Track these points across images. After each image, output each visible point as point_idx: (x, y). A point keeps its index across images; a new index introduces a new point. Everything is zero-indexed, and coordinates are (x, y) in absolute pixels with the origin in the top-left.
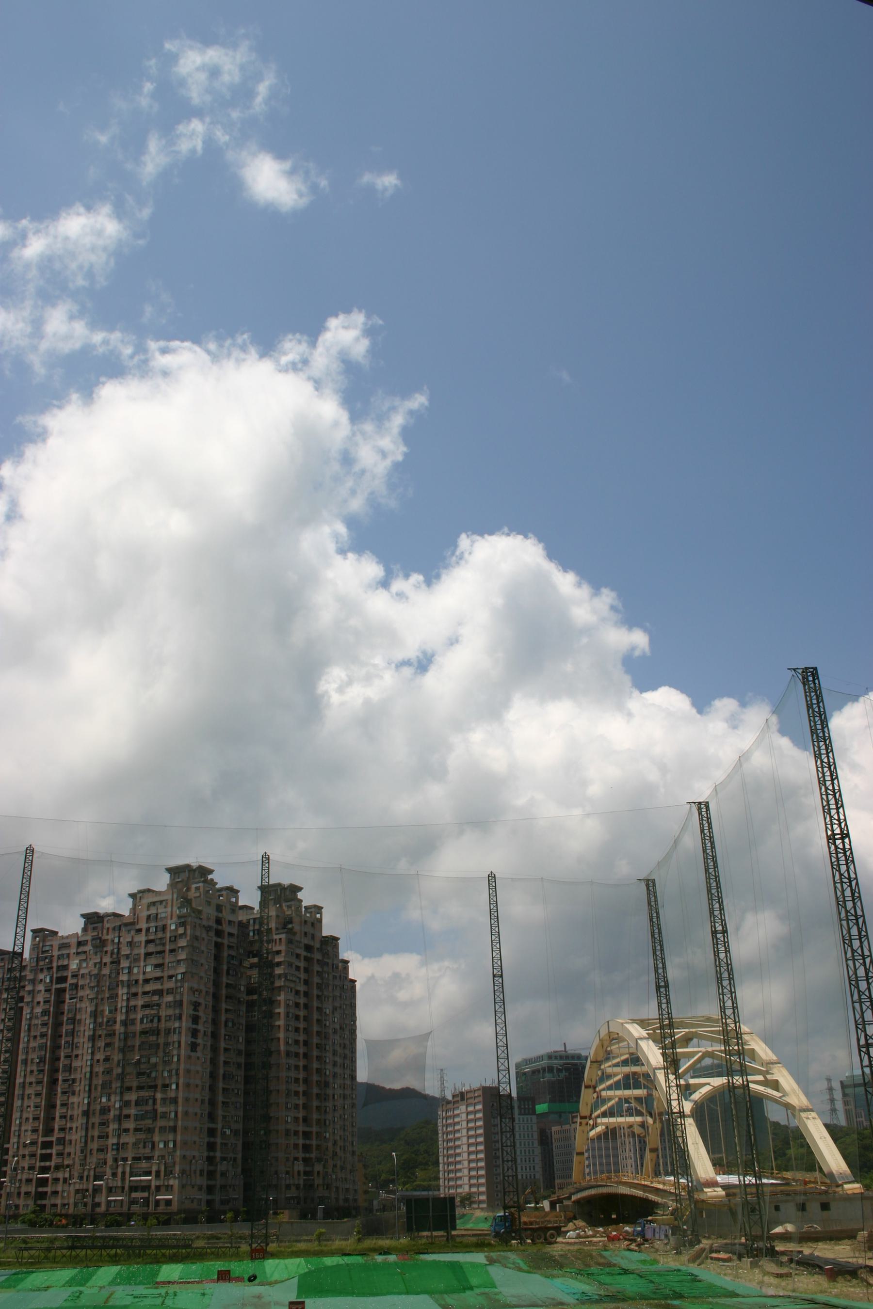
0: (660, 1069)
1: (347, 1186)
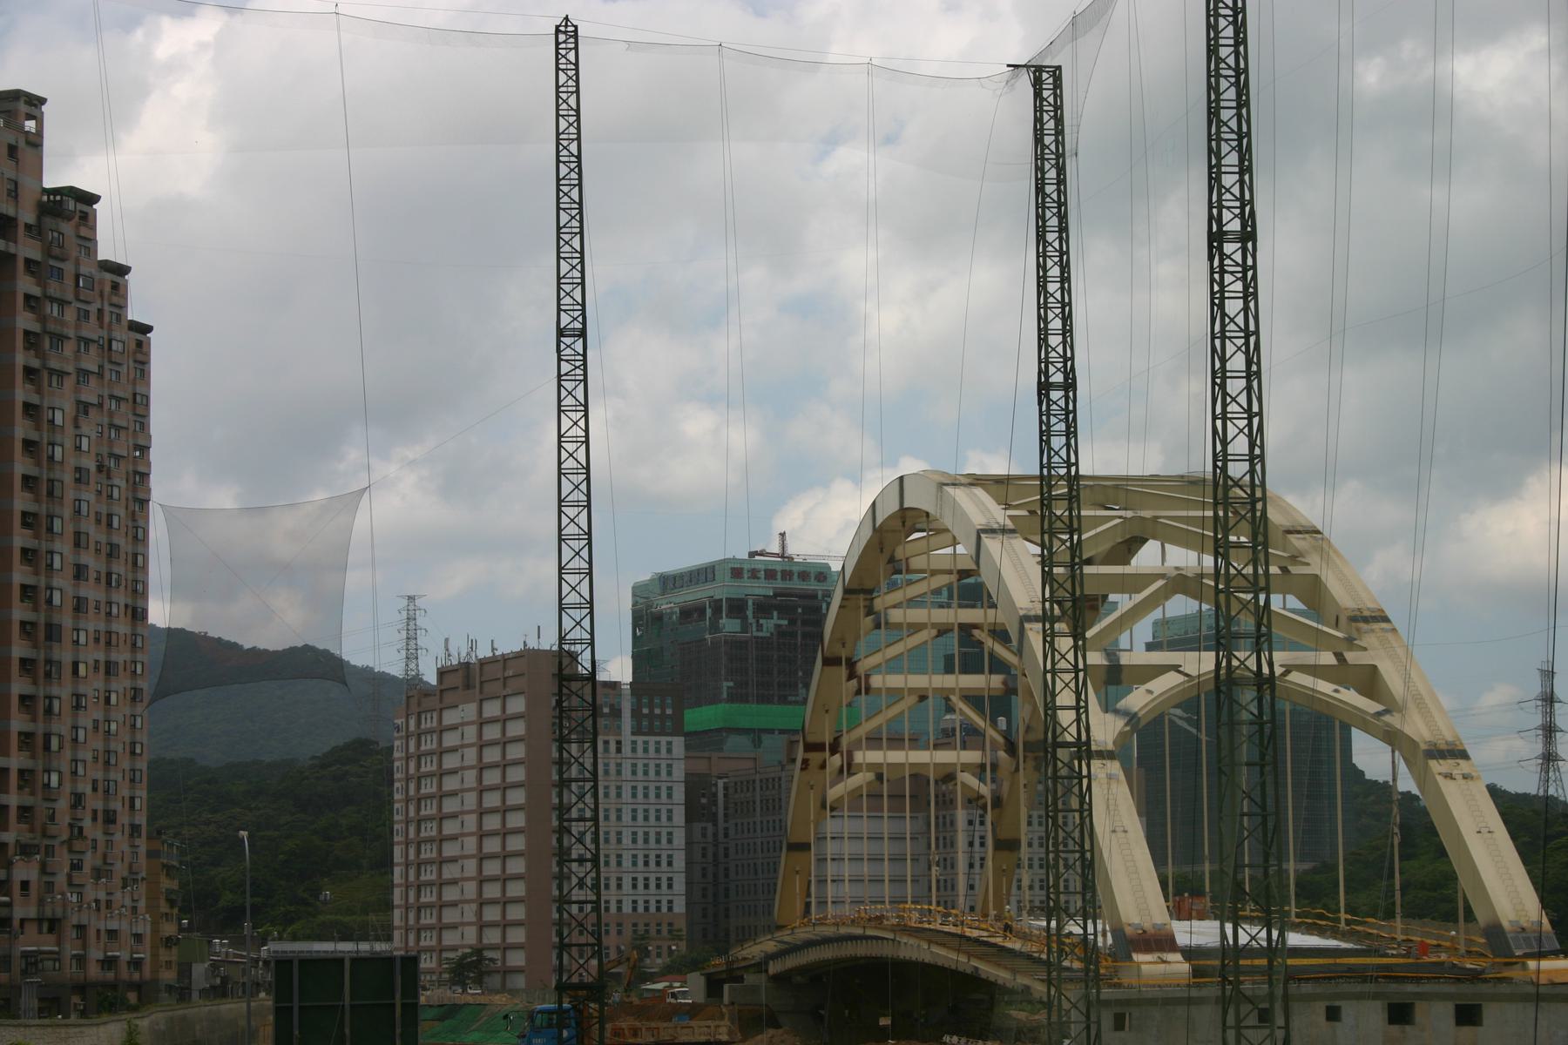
0: (1035, 619)
1: (113, 925)
